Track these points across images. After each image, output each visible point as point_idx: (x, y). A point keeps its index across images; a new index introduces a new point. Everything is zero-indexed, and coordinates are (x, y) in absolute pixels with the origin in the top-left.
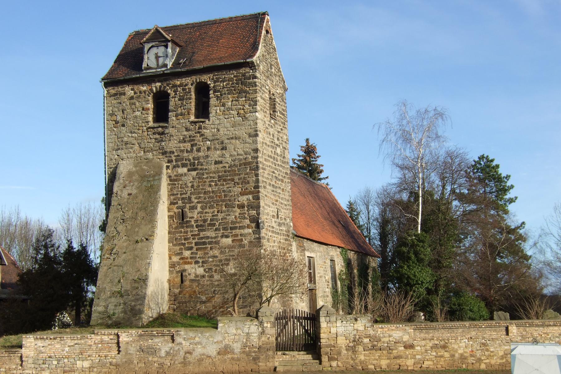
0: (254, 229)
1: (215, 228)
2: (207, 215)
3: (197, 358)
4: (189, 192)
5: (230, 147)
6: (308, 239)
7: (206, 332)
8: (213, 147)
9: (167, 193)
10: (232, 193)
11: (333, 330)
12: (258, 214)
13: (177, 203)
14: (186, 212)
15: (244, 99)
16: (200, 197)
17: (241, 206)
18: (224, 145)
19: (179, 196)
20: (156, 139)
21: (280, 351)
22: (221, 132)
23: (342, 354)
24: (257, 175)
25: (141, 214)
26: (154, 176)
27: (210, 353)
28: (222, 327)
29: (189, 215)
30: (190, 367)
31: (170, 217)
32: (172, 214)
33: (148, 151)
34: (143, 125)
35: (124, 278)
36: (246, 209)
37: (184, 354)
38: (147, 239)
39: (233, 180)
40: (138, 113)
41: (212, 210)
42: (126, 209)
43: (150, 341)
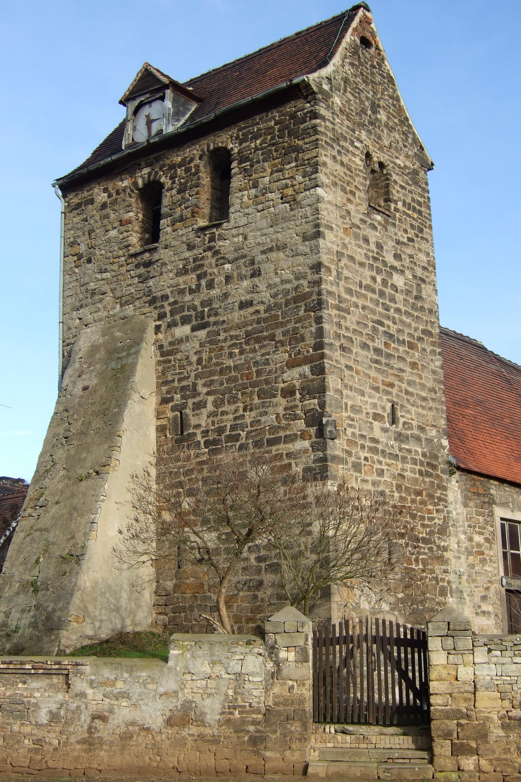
0: (314, 439)
1: (238, 444)
2: (225, 417)
3: (118, 731)
4: (193, 374)
5: (267, 268)
6: (502, 481)
7: (142, 669)
8: (235, 274)
9: (155, 380)
10: (272, 366)
11: (465, 673)
12: (322, 405)
13: (172, 399)
14: (187, 415)
15: (293, 164)
16: (212, 382)
17: (289, 392)
18: (256, 266)
19: (176, 384)
20: (139, 276)
21: (332, 722)
22: (251, 241)
23: (492, 738)
24: (319, 320)
25: (97, 423)
26: (130, 347)
27: (149, 722)
28: (177, 656)
29: (193, 421)
30: (102, 753)
31: (161, 429)
32: (164, 422)
33: (127, 303)
34: (121, 253)
35: (47, 555)
36: (298, 396)
37: (89, 719)
38: (97, 473)
39: (272, 337)
40: (113, 233)
41: (233, 407)
42: (75, 416)
43: (20, 685)
